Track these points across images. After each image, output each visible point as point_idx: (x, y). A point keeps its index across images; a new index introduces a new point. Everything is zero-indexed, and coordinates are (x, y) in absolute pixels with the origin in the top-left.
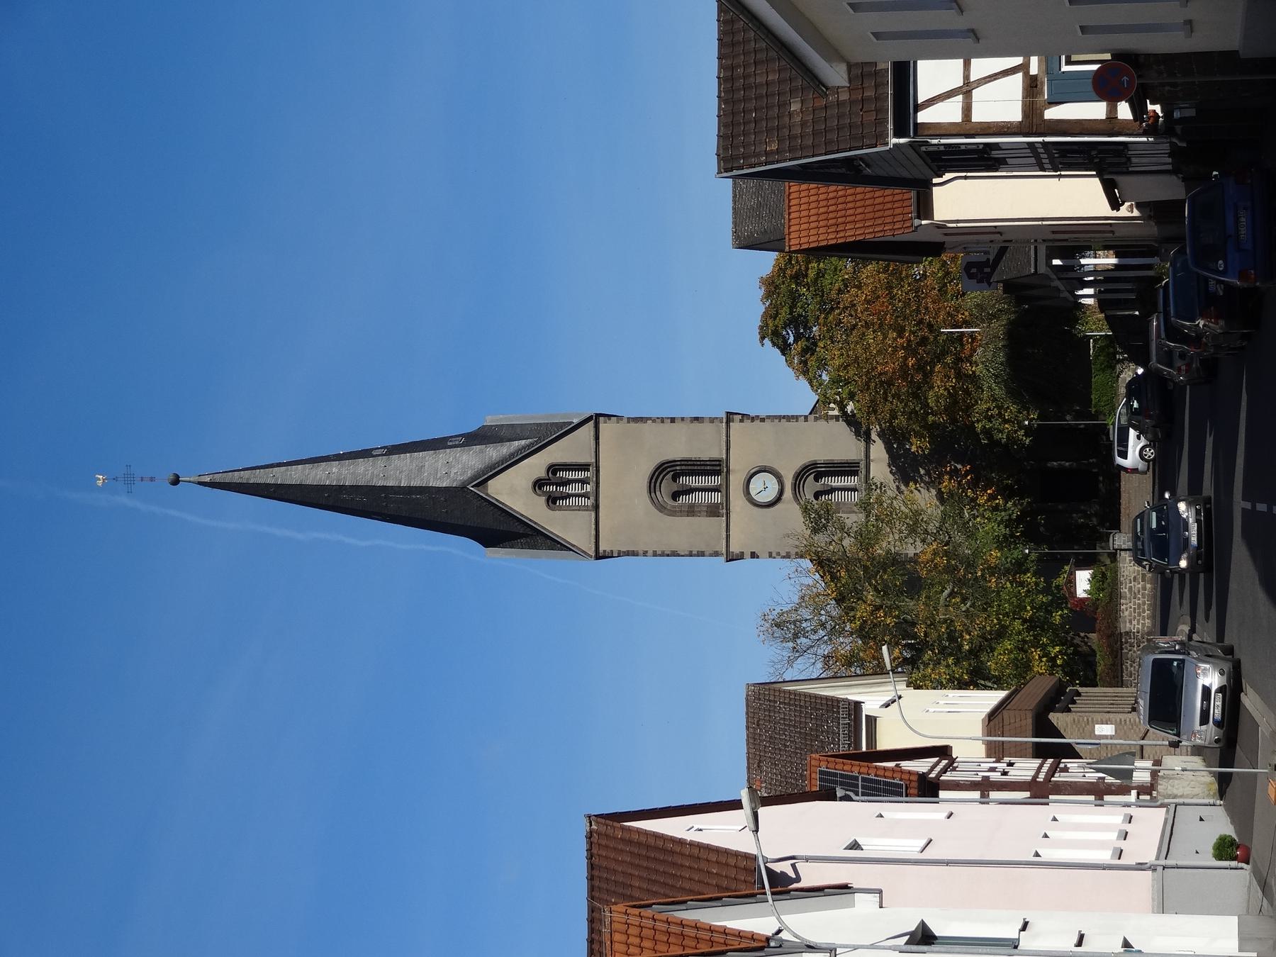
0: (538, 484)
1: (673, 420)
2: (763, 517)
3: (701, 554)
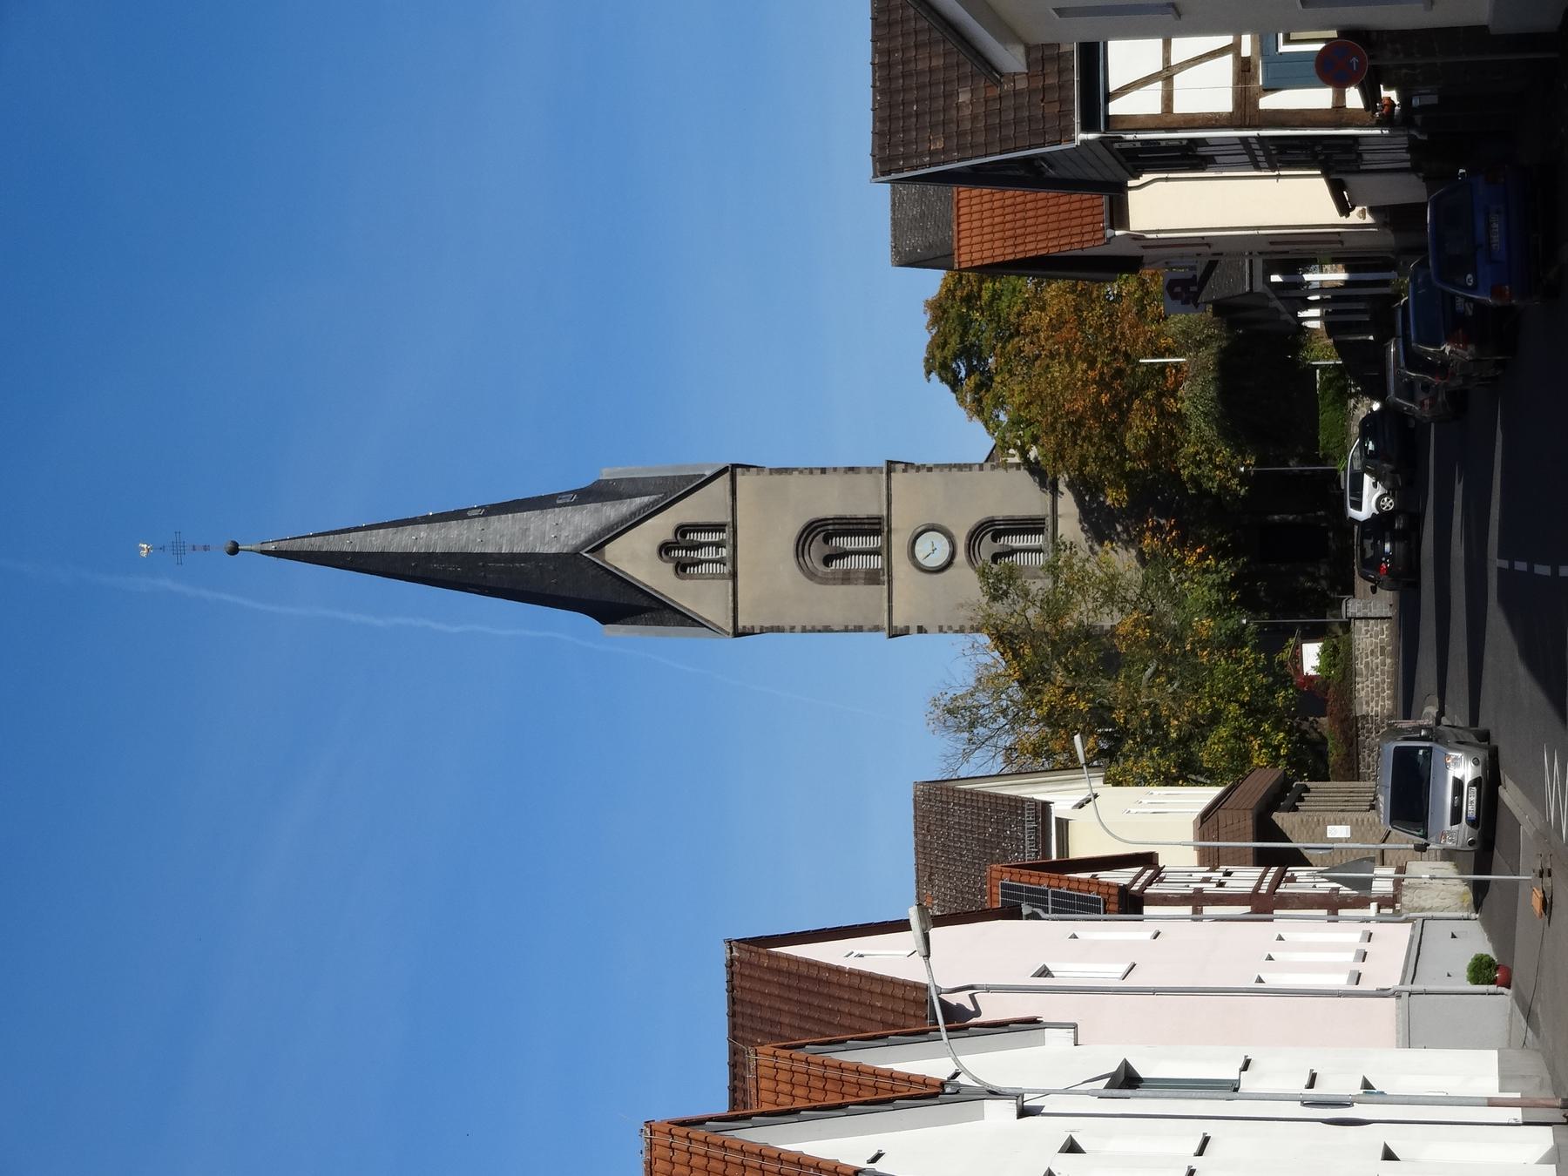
0: (665, 549)
1: (823, 471)
2: (932, 582)
3: (859, 629)
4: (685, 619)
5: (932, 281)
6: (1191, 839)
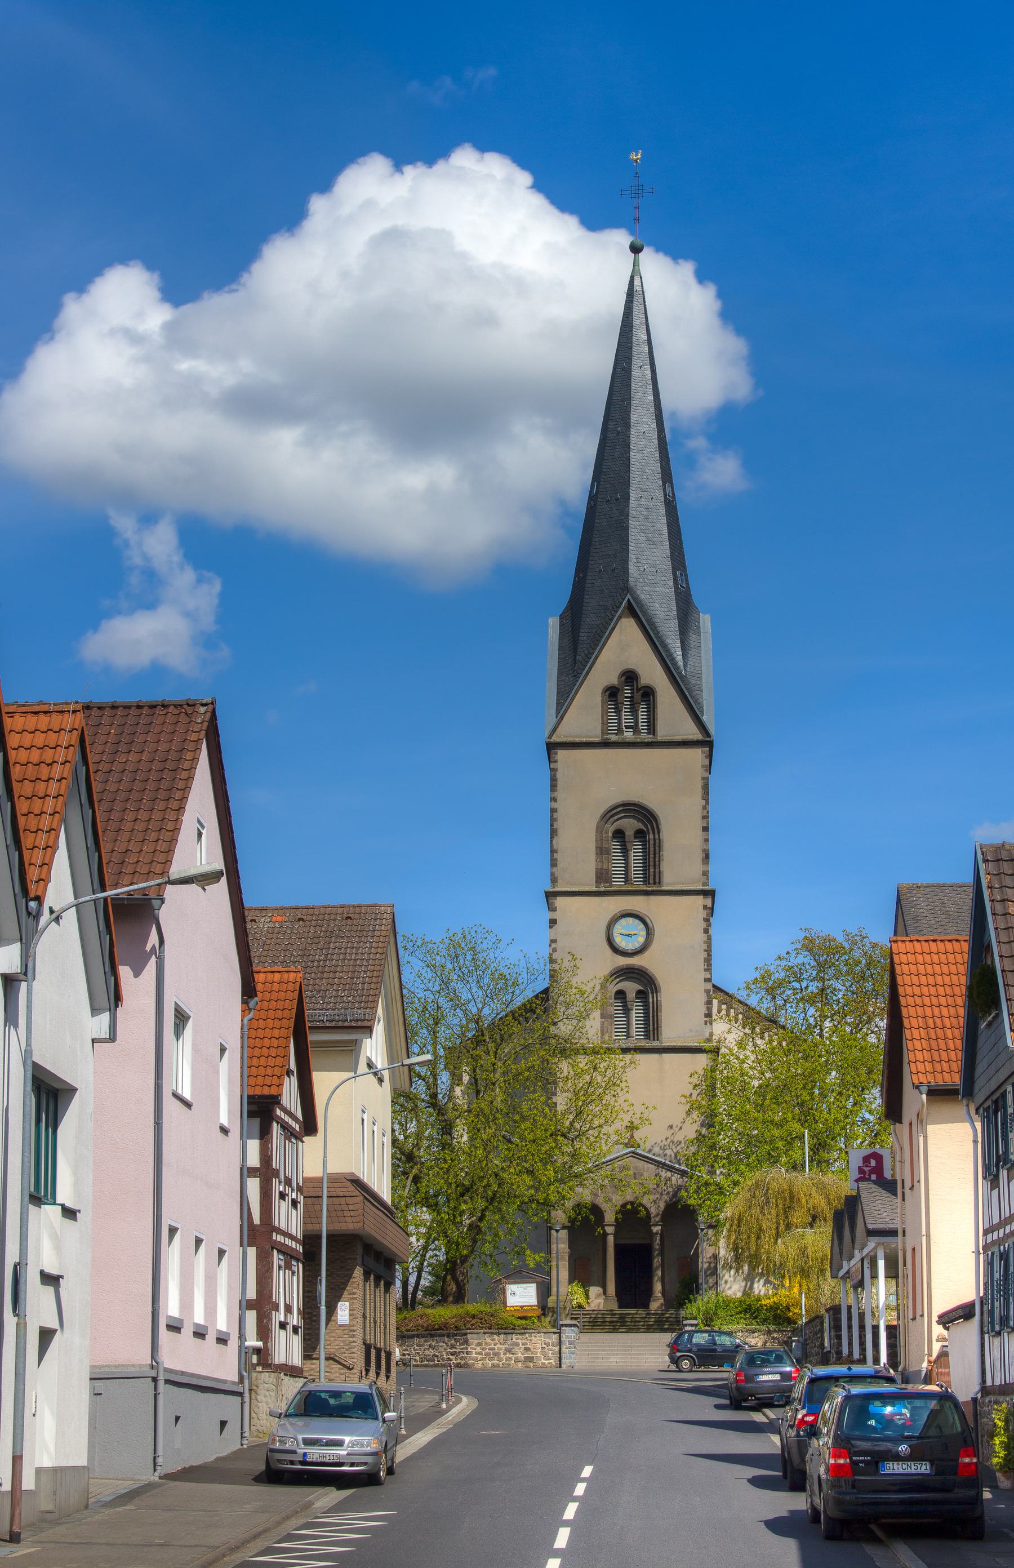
0: (630, 676)
1: (706, 829)
3: (554, 863)
4: (565, 695)
5: (880, 933)
6: (331, 1169)
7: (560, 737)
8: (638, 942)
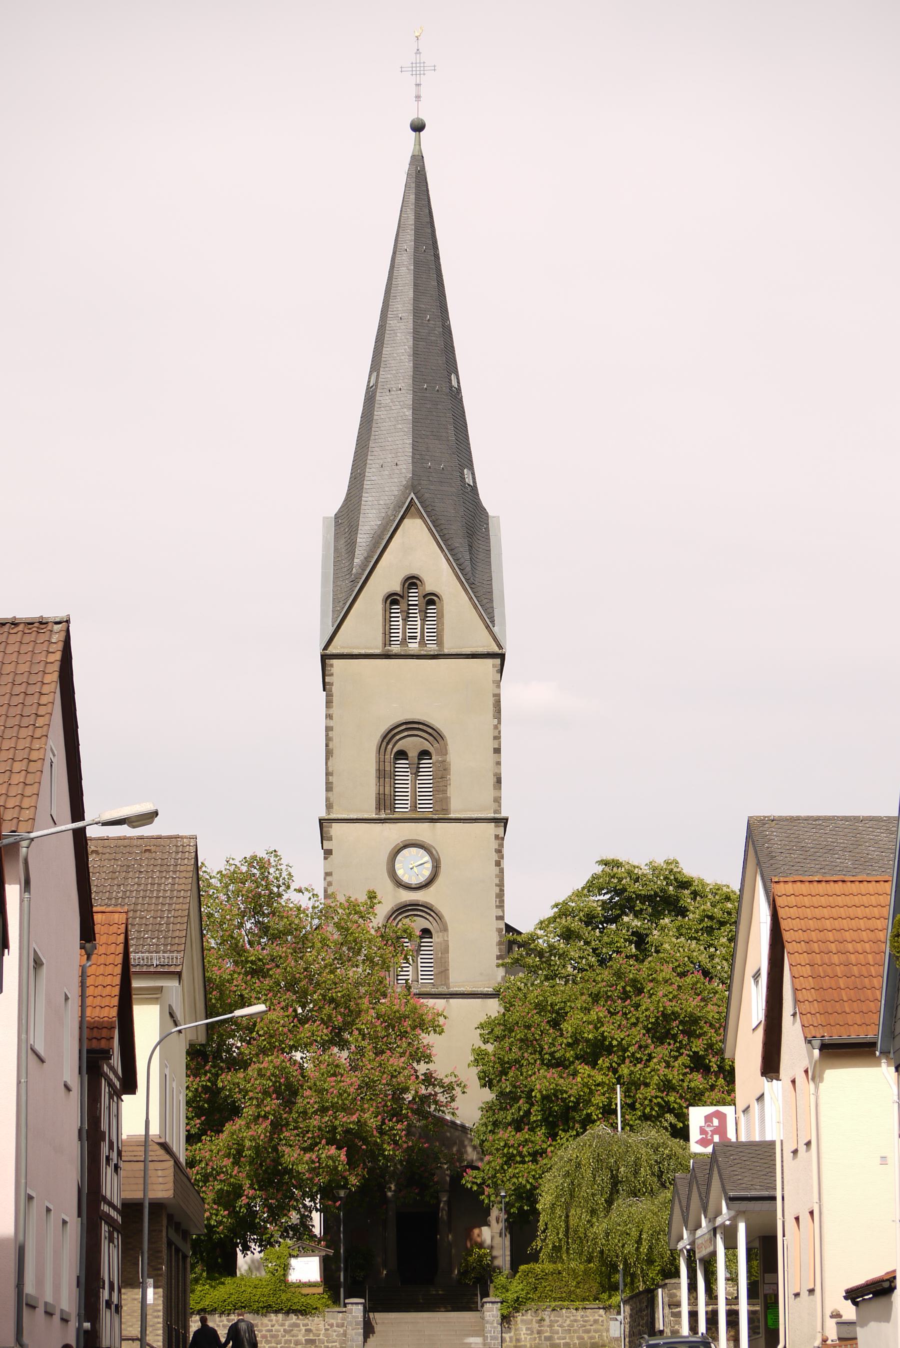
1: (497, 751)
2: (369, 866)
3: (329, 787)
7: (336, 648)
8: (423, 875)
